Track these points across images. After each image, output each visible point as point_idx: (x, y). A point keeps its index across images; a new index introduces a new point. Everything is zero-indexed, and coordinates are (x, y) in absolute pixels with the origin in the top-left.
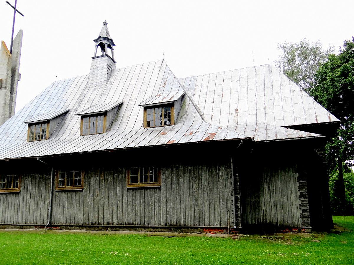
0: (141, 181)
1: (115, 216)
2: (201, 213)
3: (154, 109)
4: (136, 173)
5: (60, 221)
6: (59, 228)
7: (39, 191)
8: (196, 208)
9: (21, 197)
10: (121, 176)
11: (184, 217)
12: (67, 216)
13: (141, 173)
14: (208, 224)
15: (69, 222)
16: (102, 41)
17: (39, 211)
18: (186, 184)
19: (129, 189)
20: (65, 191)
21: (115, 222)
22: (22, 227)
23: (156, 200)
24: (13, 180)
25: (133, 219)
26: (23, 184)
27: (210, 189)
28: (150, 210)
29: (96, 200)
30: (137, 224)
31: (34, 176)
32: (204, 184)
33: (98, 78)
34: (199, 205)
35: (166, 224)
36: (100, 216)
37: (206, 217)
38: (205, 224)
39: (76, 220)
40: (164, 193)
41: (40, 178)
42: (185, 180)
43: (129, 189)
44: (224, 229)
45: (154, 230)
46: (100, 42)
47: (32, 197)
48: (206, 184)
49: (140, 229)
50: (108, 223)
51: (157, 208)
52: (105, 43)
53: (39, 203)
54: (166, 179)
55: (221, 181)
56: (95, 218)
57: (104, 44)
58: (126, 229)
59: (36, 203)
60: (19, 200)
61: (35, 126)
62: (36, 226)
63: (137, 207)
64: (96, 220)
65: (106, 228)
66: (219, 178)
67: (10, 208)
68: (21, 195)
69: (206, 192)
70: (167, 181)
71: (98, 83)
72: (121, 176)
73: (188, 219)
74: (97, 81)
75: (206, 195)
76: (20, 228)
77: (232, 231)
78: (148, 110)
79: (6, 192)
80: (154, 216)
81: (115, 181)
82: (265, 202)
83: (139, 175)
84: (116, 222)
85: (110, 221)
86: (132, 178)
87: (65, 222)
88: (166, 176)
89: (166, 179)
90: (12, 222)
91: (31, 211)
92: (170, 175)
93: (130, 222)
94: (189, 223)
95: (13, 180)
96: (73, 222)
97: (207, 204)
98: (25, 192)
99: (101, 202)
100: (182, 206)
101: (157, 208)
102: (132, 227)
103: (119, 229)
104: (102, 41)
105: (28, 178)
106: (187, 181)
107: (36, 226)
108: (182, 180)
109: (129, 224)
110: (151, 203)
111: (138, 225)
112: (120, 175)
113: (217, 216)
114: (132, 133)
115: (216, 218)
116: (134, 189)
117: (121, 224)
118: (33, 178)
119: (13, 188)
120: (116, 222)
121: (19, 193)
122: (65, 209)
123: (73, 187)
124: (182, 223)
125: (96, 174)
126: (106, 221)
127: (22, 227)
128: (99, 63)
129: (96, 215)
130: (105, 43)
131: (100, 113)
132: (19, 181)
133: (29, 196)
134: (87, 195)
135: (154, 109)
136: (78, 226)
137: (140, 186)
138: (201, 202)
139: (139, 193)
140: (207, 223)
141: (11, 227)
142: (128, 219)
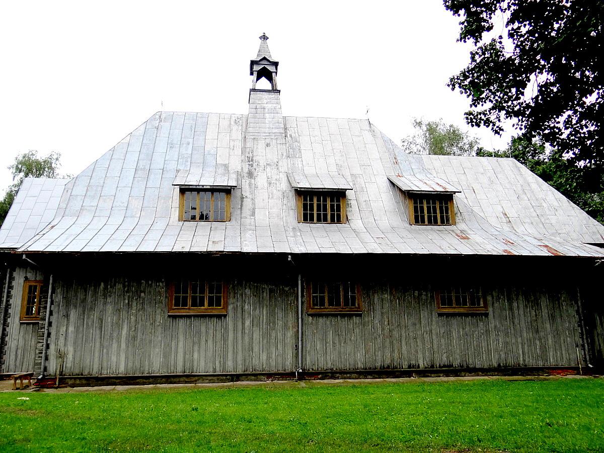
0: (194, 304)
1: (420, 355)
2: (544, 349)
3: (212, 194)
4: (202, 292)
5: (320, 365)
6: (320, 376)
7: (272, 314)
8: (538, 342)
9: (231, 327)
10: (425, 295)
11: (523, 355)
12: (334, 356)
13: (195, 292)
14: (554, 364)
15: (339, 366)
16: (266, 66)
17: (274, 350)
18: (522, 312)
19: (440, 315)
20: (327, 316)
21: (422, 365)
22: (236, 378)
23: (482, 331)
24: (207, 291)
25: (451, 358)
26: (231, 300)
27: (552, 318)
28: (475, 345)
29: (386, 331)
30: (457, 366)
31: (257, 286)
32: (545, 312)
33: (267, 126)
34: (540, 339)
35: (215, 370)
36: (396, 355)
37: (551, 354)
38: (551, 364)
39: (352, 362)
40: (493, 322)
41: (271, 291)
42: (520, 307)
43: (169, 316)
44: (575, 370)
45: (483, 374)
46: (263, 66)
47: (255, 323)
48: (546, 311)
49: (463, 374)
50: (410, 367)
51: (484, 342)
52: (264, 69)
53: (273, 335)
54: (493, 303)
55: (564, 307)
56: (382, 358)
57: (272, 72)
58: (441, 375)
59: (266, 335)
60: (226, 329)
61: (204, 193)
62: (269, 376)
63: (454, 341)
64: (388, 362)
65: (407, 374)
66: (562, 304)
67: (203, 342)
68: (230, 320)
69: (548, 322)
70: (496, 305)
71: (268, 134)
72: (425, 295)
73: (529, 357)
74: (267, 130)
75: (548, 326)
76: (232, 381)
77: (587, 371)
78: (188, 193)
79: (192, 313)
80: (483, 354)
81: (416, 302)
82: (598, 335)
83: (189, 294)
84: (424, 364)
85: (413, 362)
86: (177, 299)
87: (329, 366)
88: (493, 298)
89: (493, 303)
90: (212, 370)
91: (256, 349)
92: (498, 299)
93: (446, 364)
94: (531, 362)
95: (207, 291)
96: (347, 365)
97: (550, 337)
98: (239, 315)
99: (396, 334)
100: (519, 340)
101: (484, 342)
102: (449, 370)
103: (429, 375)
104: (266, 66)
105: (246, 289)
106: (521, 306)
107: (269, 376)
108: (515, 304)
109: (445, 366)
110: (475, 336)
111: (458, 367)
112: (424, 293)
113: (564, 352)
114: (268, 227)
115: (564, 355)
116: (448, 315)
117: (432, 366)
118: (257, 293)
119: (209, 306)
120: (424, 364)
121: (225, 316)
122: (328, 344)
123: (343, 308)
124: (522, 362)
125: (383, 291)
126: (406, 363)
127: (236, 378)
128: (265, 101)
129: (388, 354)
130: (264, 69)
131: (324, 190)
132: (222, 295)
133: (247, 323)
134: (368, 322)
135: (212, 194)
136: (357, 373)
137: (457, 311)
138: (542, 334)
139: (455, 322)
140: (552, 362)
141: (210, 380)
142: (442, 359)
